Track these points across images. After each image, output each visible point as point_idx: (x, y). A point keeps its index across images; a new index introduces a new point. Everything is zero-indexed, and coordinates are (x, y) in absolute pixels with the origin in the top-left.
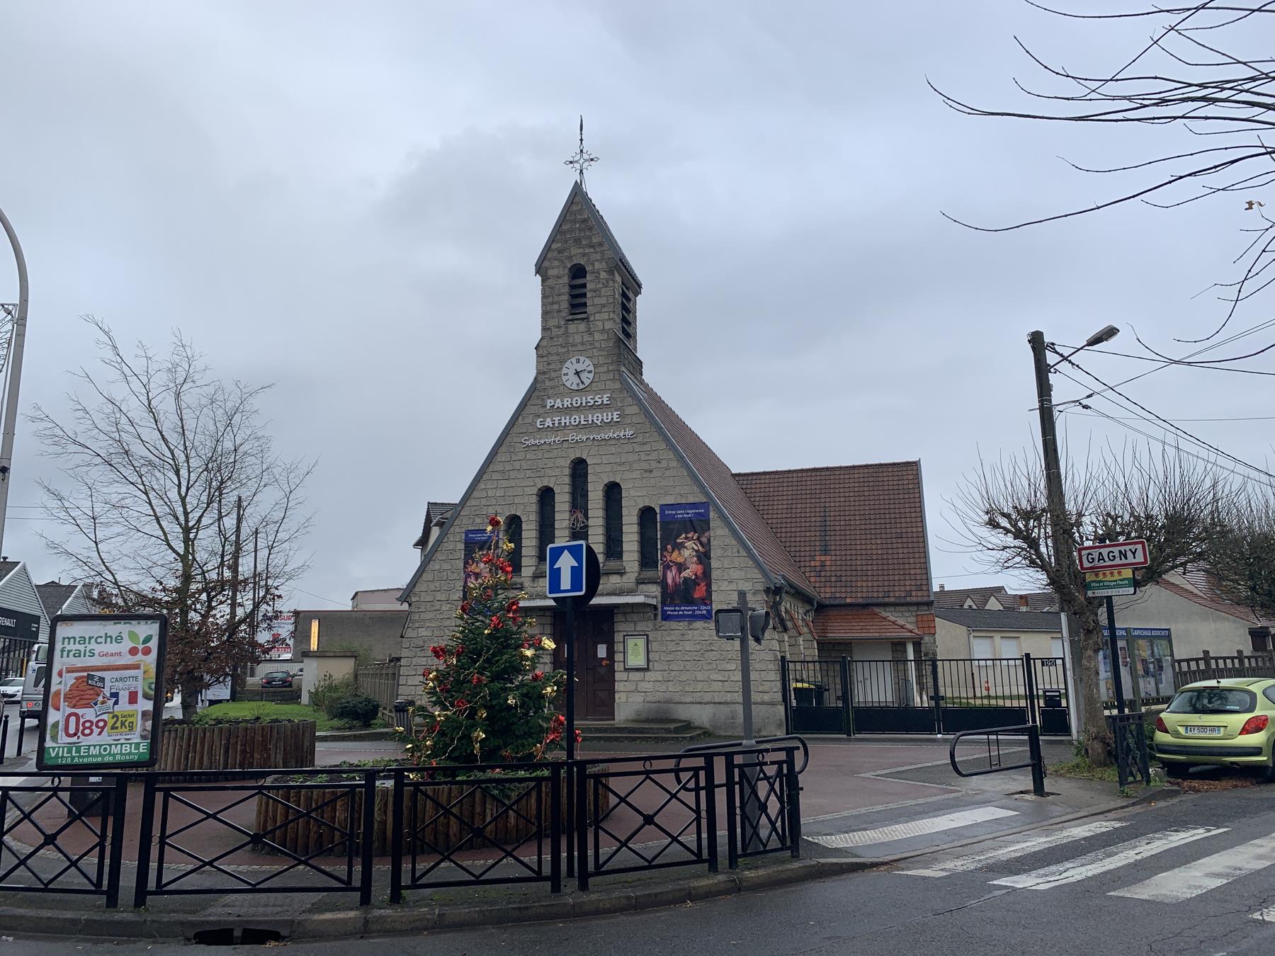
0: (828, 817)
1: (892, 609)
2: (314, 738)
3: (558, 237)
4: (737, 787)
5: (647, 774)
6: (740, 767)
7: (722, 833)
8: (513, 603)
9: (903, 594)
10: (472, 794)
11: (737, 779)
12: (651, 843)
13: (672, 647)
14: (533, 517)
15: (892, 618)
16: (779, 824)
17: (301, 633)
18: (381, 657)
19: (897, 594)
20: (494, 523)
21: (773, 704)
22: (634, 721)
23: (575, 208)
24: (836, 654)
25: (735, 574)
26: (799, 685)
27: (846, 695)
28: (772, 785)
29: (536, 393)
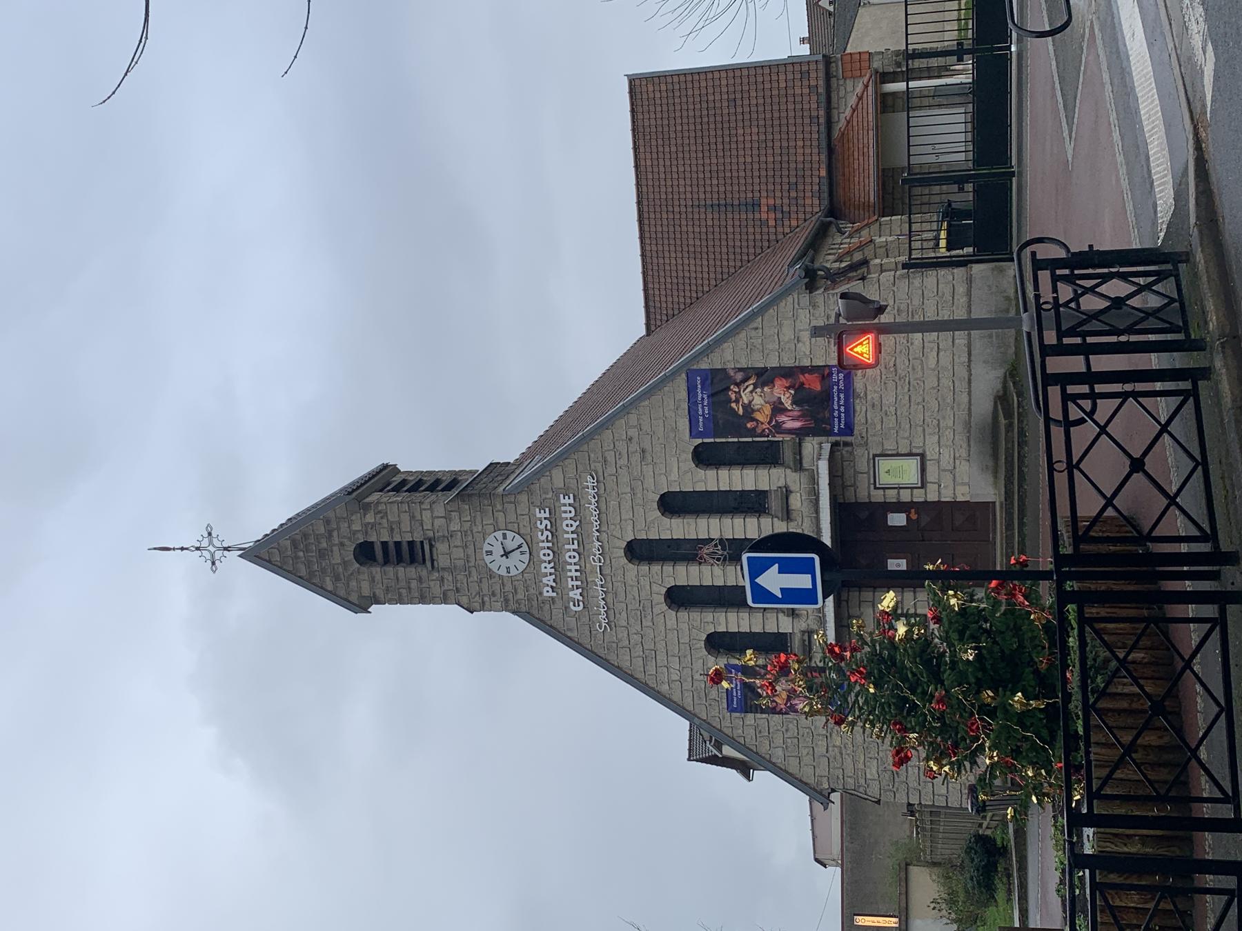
0: (1129, 207)
1: (835, 112)
4: (1090, 340)
5: (1072, 467)
6: (1061, 334)
7: (1154, 361)
8: (832, 651)
10: (1100, 713)
11: (1078, 340)
12: (1171, 463)
13: (891, 422)
14: (708, 616)
15: (848, 112)
16: (1141, 281)
18: (907, 826)
19: (814, 106)
20: (717, 677)
21: (970, 280)
22: (996, 476)
23: (277, 558)
24: (899, 189)
25: (788, 333)
26: (943, 243)
27: (959, 180)
28: (1087, 291)
29: (535, 612)
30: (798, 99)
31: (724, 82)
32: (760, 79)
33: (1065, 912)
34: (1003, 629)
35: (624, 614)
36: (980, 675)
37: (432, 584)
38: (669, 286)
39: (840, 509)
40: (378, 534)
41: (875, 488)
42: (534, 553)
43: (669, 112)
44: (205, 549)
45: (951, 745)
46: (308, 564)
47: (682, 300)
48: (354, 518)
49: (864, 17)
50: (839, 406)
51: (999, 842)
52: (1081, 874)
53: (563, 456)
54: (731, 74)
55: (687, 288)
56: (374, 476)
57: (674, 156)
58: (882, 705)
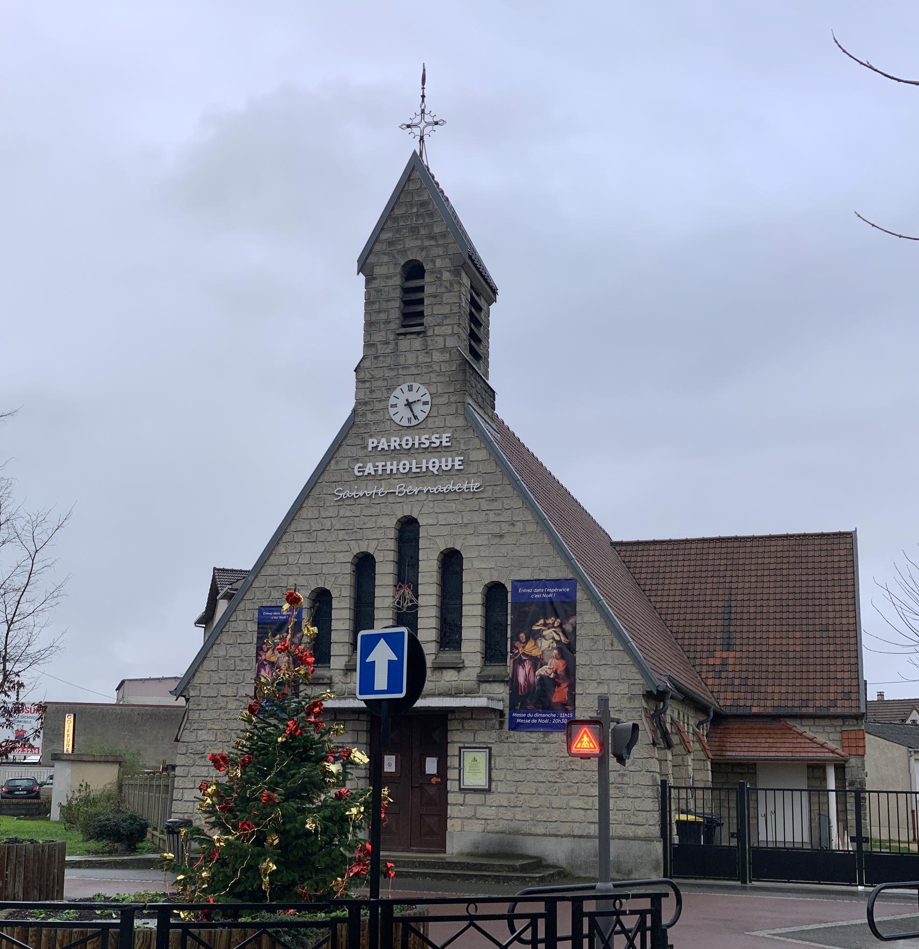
1: (811, 722)
2: (64, 865)
3: (389, 224)
5: (471, 920)
6: (591, 915)
8: (315, 705)
9: (825, 704)
10: (258, 938)
11: (586, 931)
13: (520, 764)
14: (347, 592)
15: (810, 734)
17: (52, 733)
18: (153, 764)
19: (819, 703)
20: (293, 599)
21: (648, 839)
22: (471, 855)
23: (412, 187)
24: (736, 779)
25: (606, 673)
26: (683, 817)
27: (741, 834)
29: (354, 430)
30: (825, 689)
31: (844, 621)
32: (845, 654)
33: (80, 900)
34: (333, 856)
35: (349, 514)
36: (293, 833)
37: (384, 333)
38: (656, 564)
39: (444, 714)
40: (431, 283)
41: (460, 748)
42: (409, 431)
43: (821, 568)
44: (423, 118)
45: (229, 806)
46: (404, 216)
47: (643, 576)
48: (447, 260)
49: (898, 751)
50: (537, 718)
51: (140, 845)
52: (114, 916)
53: (499, 461)
54: (852, 628)
55: (654, 582)
56: (486, 280)
57: (778, 572)
58: (265, 748)
